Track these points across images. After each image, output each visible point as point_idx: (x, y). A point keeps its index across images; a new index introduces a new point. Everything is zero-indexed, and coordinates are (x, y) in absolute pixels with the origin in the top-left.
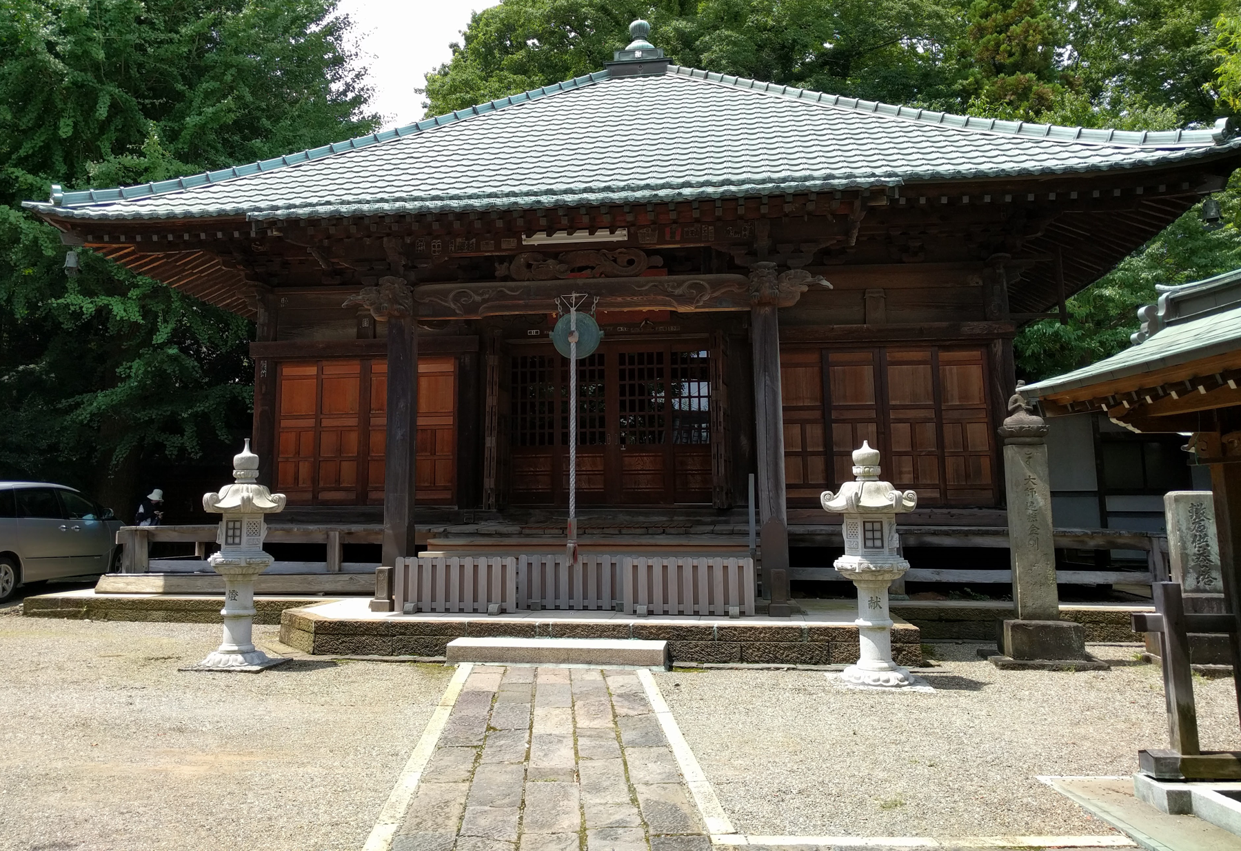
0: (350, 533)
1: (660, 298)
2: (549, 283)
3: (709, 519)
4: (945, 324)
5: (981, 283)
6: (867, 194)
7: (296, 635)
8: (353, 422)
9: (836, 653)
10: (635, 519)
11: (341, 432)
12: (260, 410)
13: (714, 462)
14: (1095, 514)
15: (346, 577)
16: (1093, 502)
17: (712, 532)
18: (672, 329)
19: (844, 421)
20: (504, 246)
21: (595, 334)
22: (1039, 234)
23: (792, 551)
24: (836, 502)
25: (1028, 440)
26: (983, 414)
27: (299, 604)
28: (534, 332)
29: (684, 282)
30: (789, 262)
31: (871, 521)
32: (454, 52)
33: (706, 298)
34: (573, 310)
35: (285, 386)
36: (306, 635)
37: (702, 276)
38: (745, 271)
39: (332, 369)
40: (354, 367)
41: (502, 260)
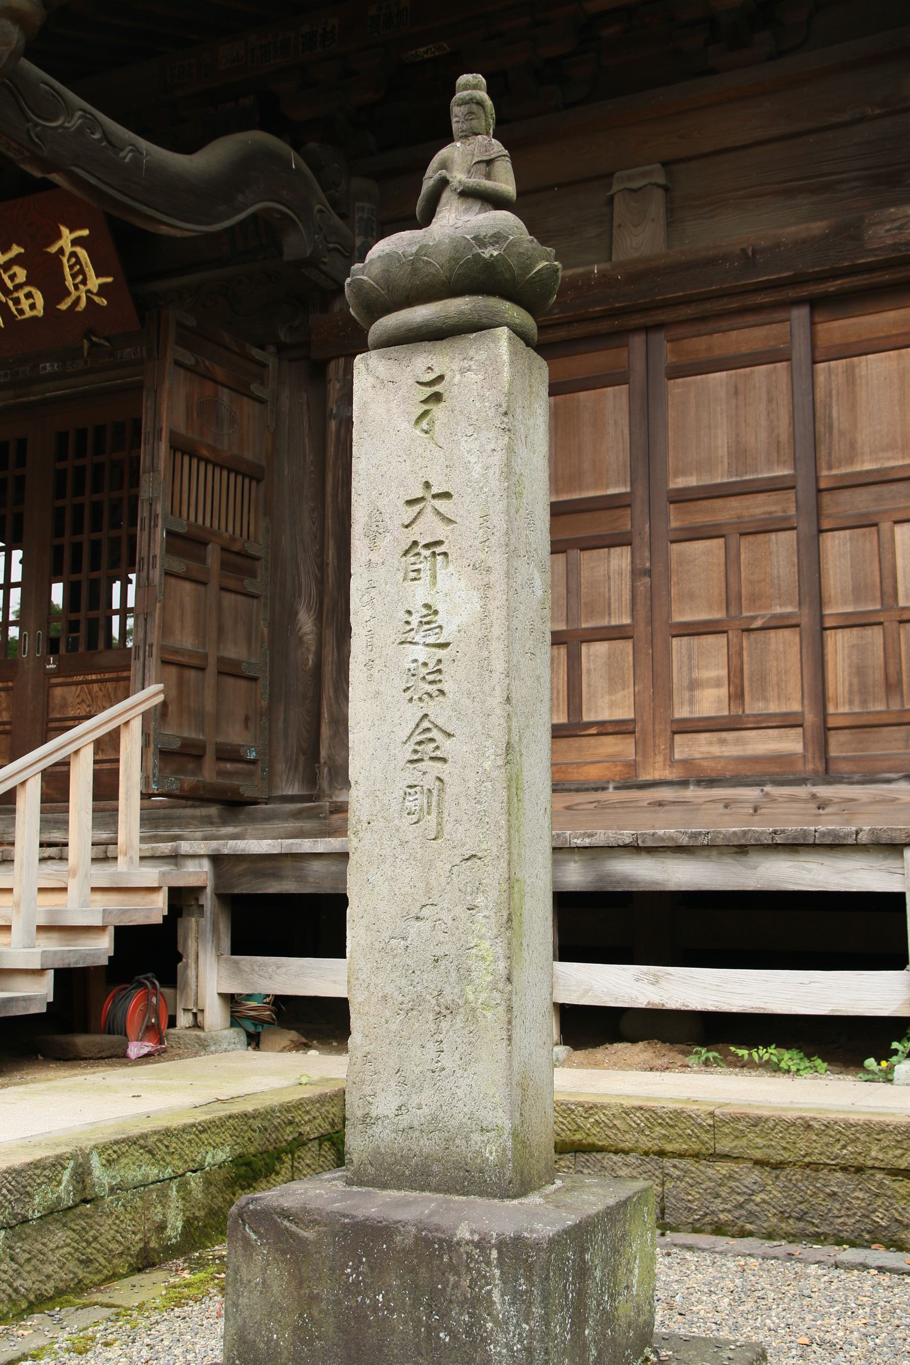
4: (818, 227)
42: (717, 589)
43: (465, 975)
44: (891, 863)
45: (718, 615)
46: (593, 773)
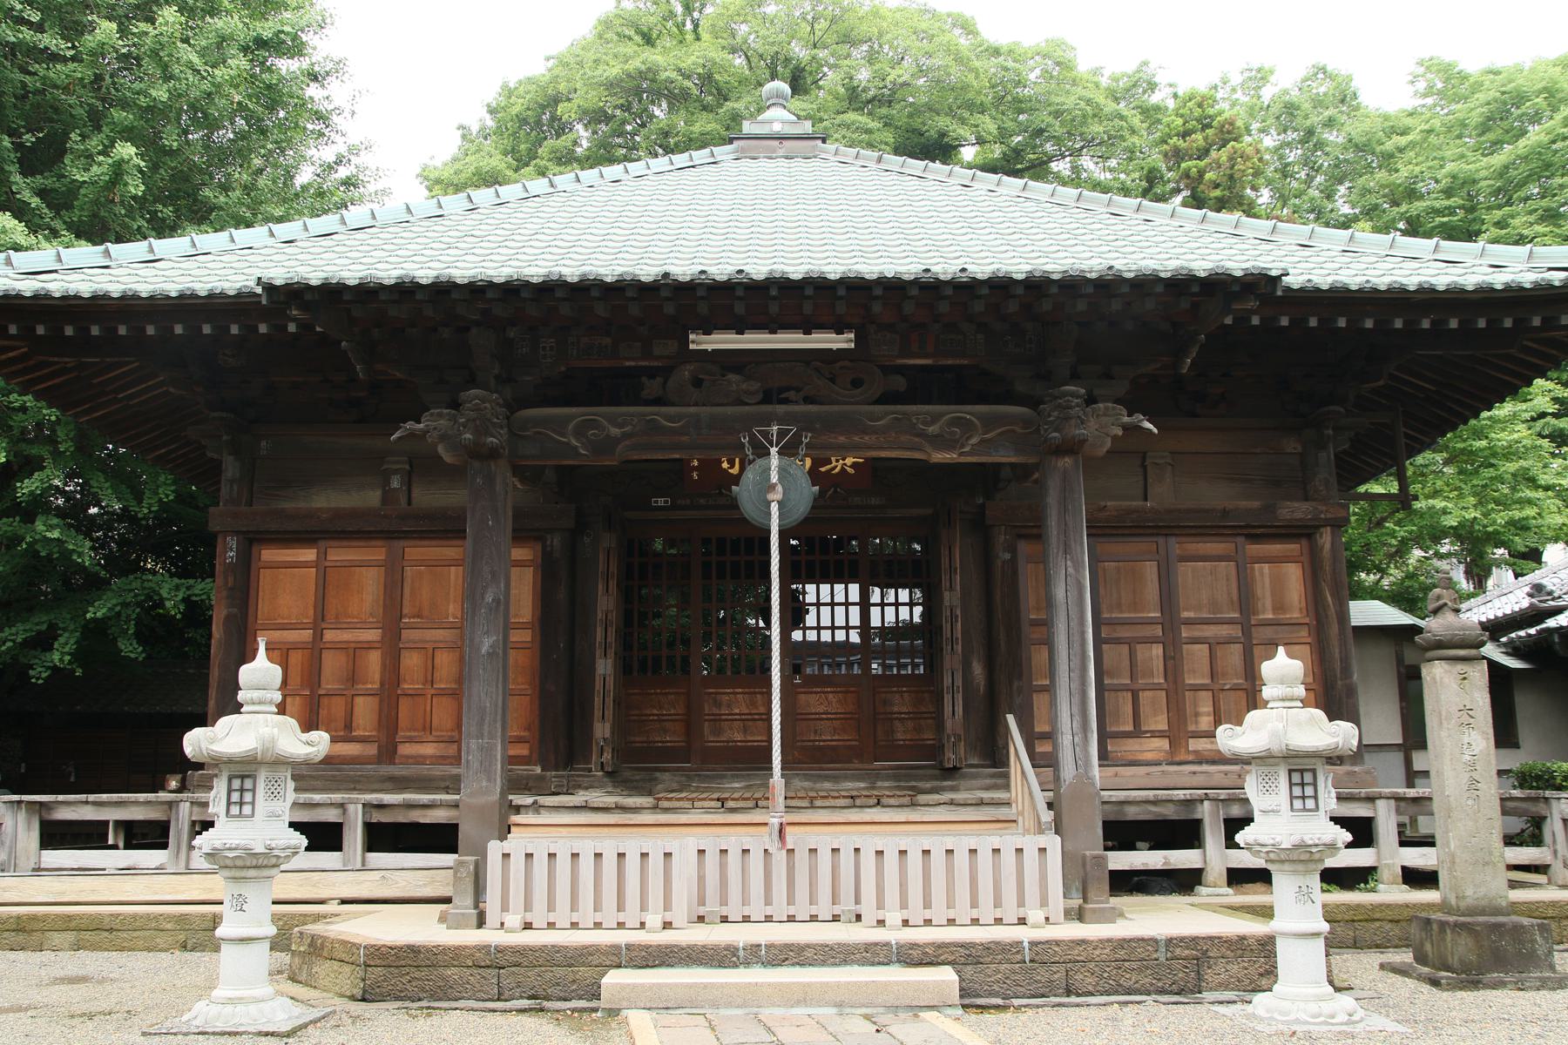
0: (381, 807)
1: (904, 438)
2: (730, 410)
3: (928, 785)
4: (1256, 504)
5: (1300, 449)
6: (1236, 288)
7: (323, 969)
8: (373, 635)
9: (1209, 975)
10: (818, 786)
11: (355, 651)
12: (224, 612)
13: (947, 699)
14: (1399, 772)
15: (376, 875)
16: (1397, 758)
17: (952, 803)
18: (874, 501)
19: (1118, 641)
20: (657, 351)
21: (807, 492)
22: (1381, 383)
23: (1107, 825)
24: (1235, 739)
25: (1462, 652)
26: (1304, 632)
27: (318, 918)
28: (661, 501)
29: (942, 415)
30: (1096, 392)
31: (1300, 768)
32: (464, 137)
33: (974, 441)
34: (773, 450)
35: (265, 577)
36: (347, 969)
37: (969, 408)
38: (1034, 403)
39: (339, 554)
40: (376, 553)
41: (652, 373)
42: (1207, 669)
43: (1491, 853)
44: (1370, 805)
45: (1207, 681)
46: (1149, 756)
